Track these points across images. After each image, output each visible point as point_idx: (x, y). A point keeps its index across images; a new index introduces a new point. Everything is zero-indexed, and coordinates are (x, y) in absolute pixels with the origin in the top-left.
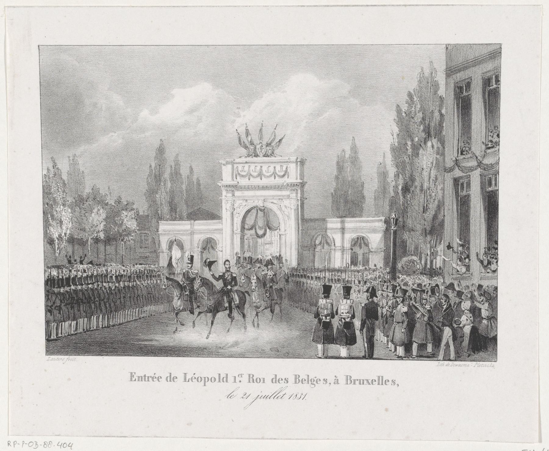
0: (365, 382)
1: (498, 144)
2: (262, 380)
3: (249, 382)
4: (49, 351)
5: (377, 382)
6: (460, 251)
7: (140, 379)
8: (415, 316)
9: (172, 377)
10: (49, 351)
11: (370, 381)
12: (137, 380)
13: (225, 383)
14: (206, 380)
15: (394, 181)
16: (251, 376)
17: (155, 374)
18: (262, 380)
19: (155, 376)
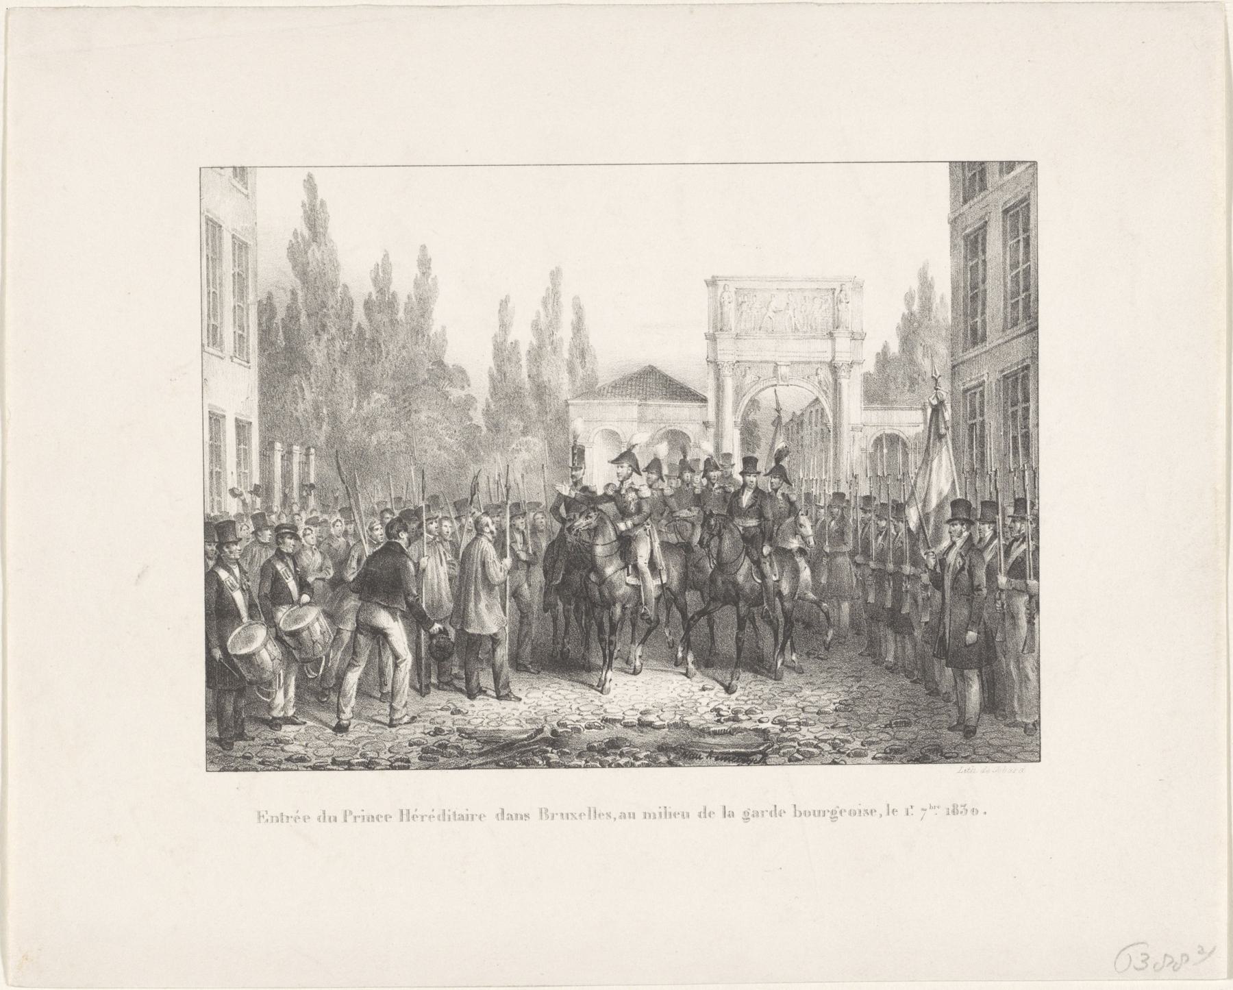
0: (570, 816)
1: (1037, 327)
2: (652, 815)
3: (402, 820)
4: (1032, 753)
5: (587, 817)
6: (481, 661)
7: (511, 817)
8: (505, 740)
9: (707, 812)
10: (1032, 753)
11: (577, 816)
12: (270, 821)
13: (333, 823)
14: (773, 813)
15: (474, 530)
16: (543, 811)
17: (298, 812)
18: (652, 815)
19: (299, 814)
